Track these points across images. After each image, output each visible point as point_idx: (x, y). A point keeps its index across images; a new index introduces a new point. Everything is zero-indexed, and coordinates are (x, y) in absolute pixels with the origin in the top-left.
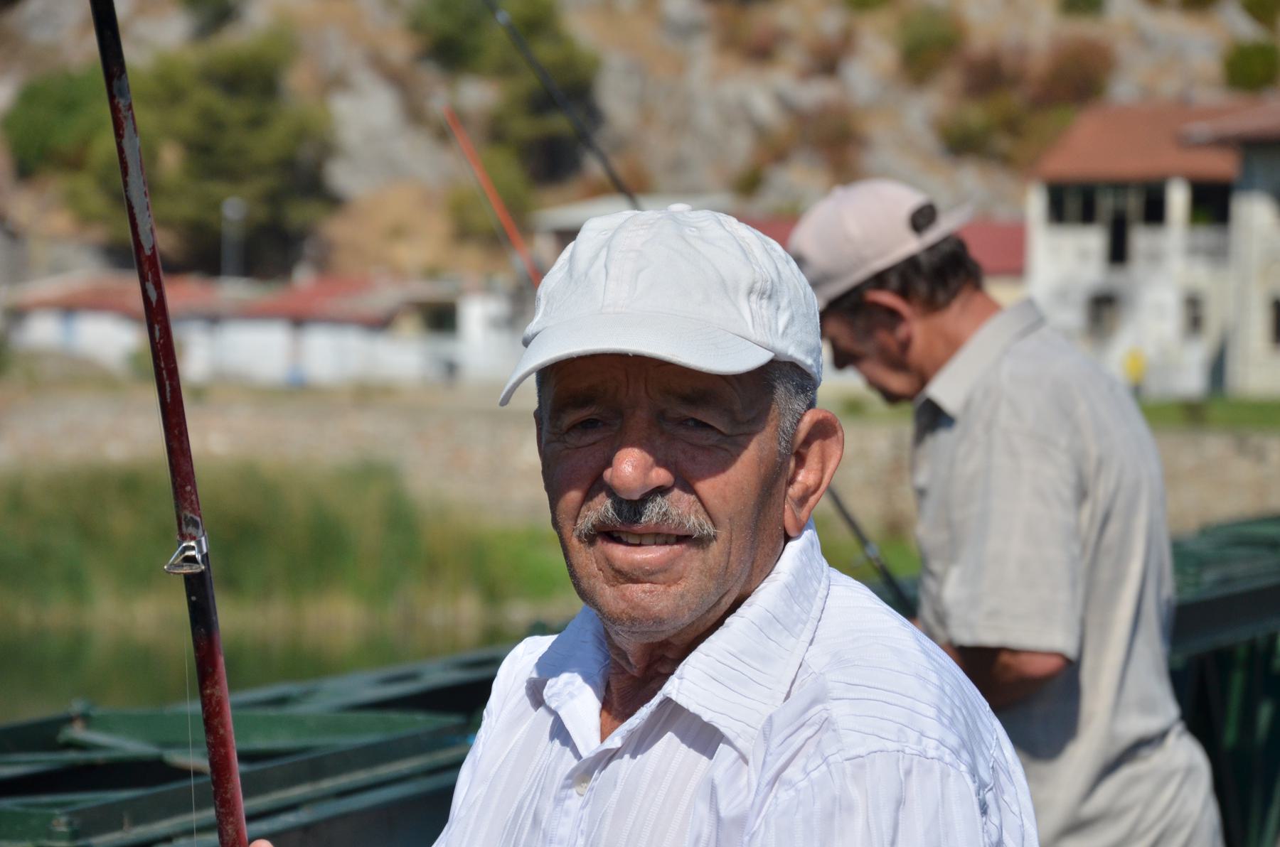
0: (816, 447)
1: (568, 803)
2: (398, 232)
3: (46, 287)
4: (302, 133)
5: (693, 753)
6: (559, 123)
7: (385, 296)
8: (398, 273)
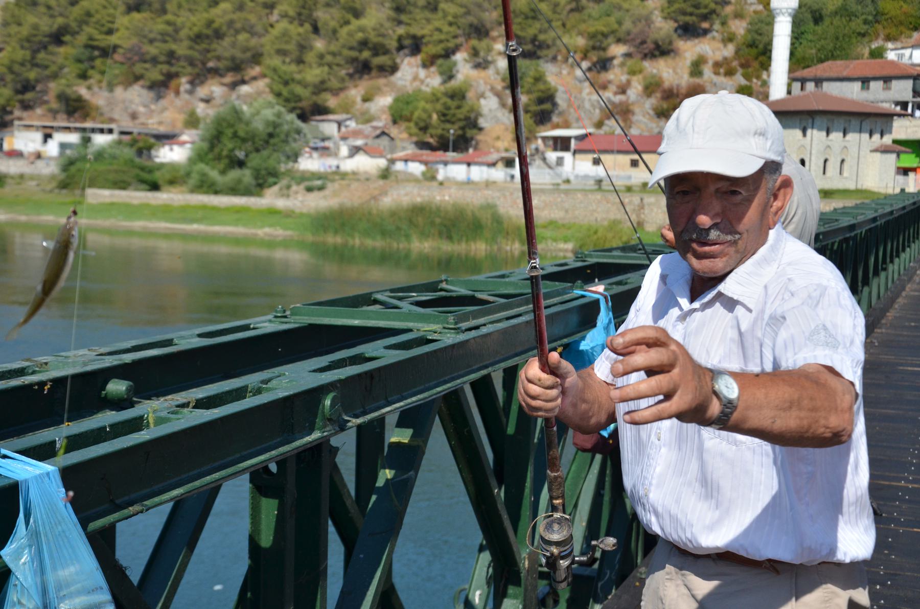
0: (782, 191)
1: (678, 327)
2: (498, 138)
3: (401, 154)
4: (472, 110)
5: (726, 312)
6: (547, 106)
7: (494, 157)
8: (498, 151)
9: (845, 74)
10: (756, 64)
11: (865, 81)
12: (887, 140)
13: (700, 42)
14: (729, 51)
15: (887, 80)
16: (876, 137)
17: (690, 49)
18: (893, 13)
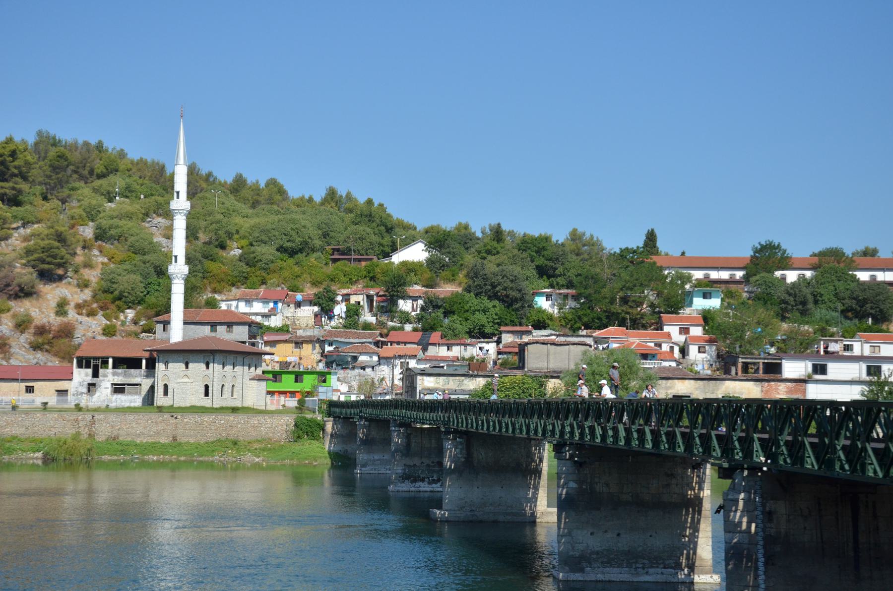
9: (197, 319)
10: (113, 307)
11: (213, 325)
12: (259, 371)
13: (57, 287)
14: (87, 294)
15: (230, 325)
16: (253, 369)
17: (52, 293)
18: (215, 272)
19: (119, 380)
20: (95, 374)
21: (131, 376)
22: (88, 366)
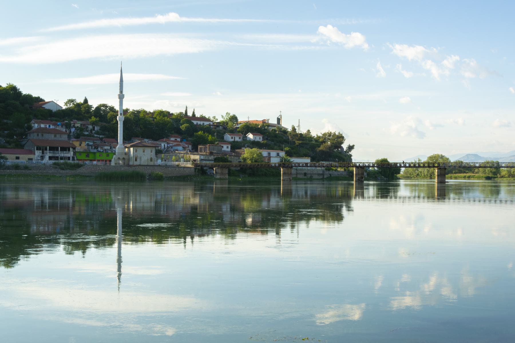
19: (51, 155)
20: (43, 153)
21: (55, 153)
22: (40, 150)
